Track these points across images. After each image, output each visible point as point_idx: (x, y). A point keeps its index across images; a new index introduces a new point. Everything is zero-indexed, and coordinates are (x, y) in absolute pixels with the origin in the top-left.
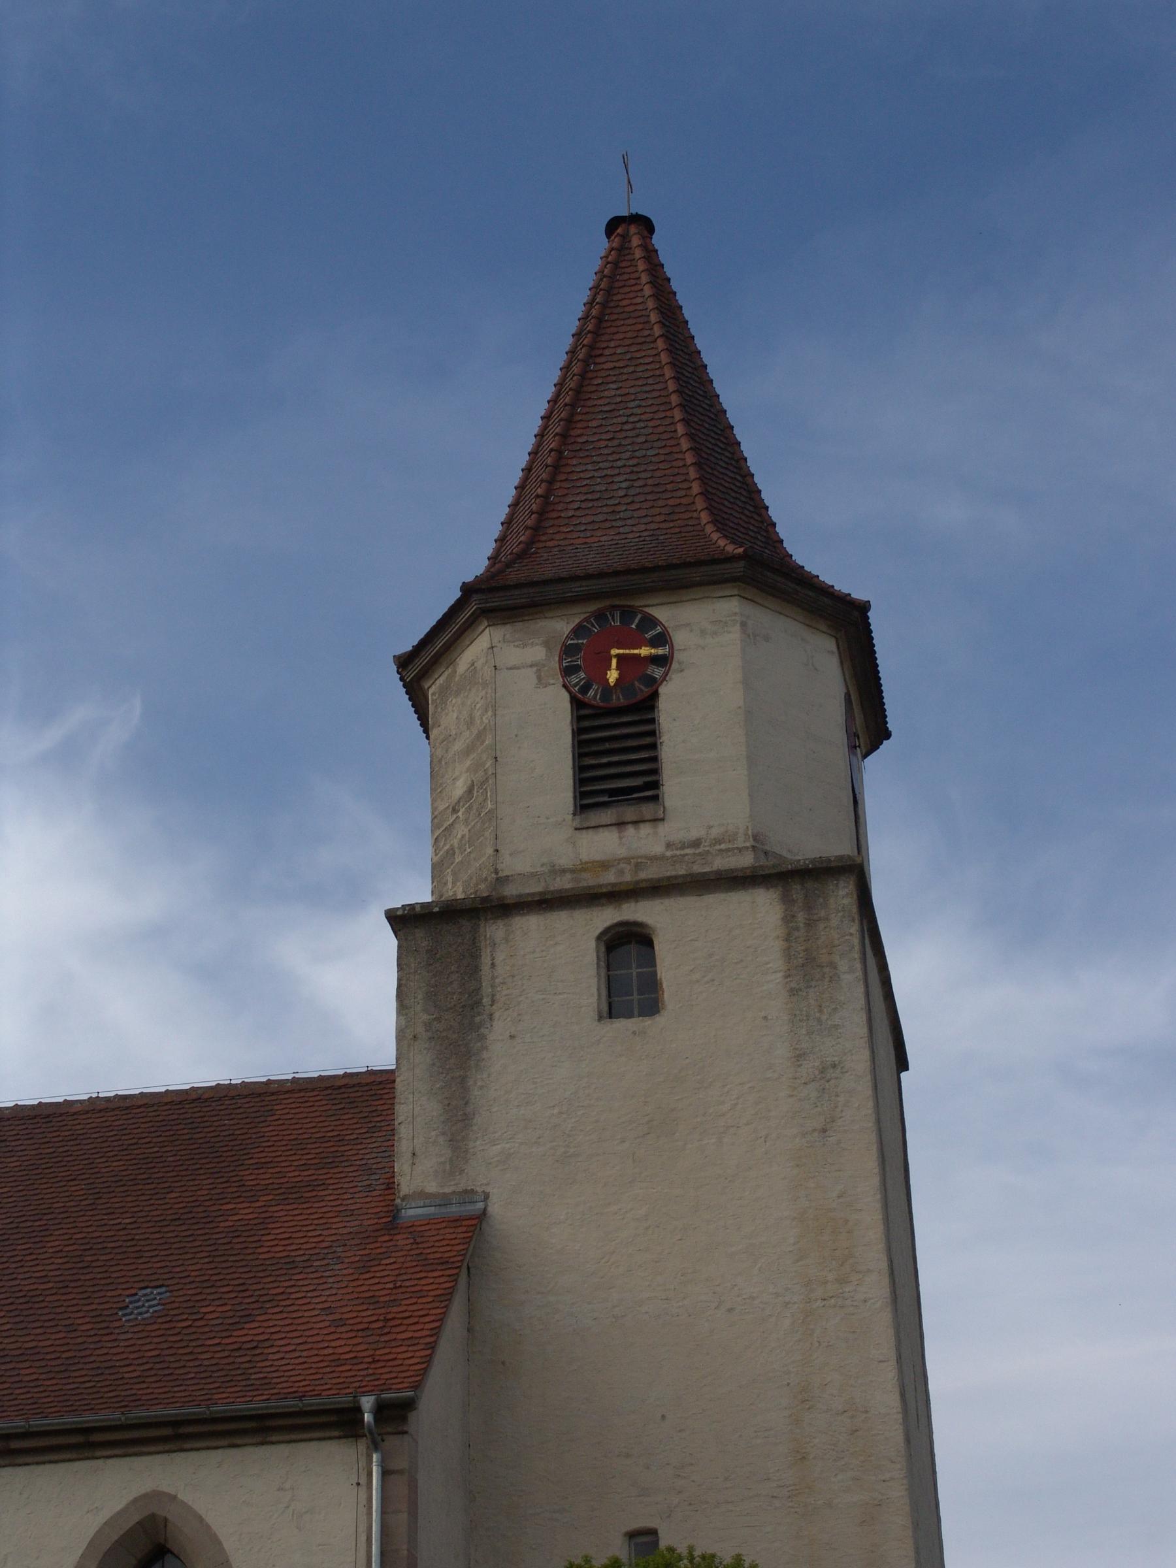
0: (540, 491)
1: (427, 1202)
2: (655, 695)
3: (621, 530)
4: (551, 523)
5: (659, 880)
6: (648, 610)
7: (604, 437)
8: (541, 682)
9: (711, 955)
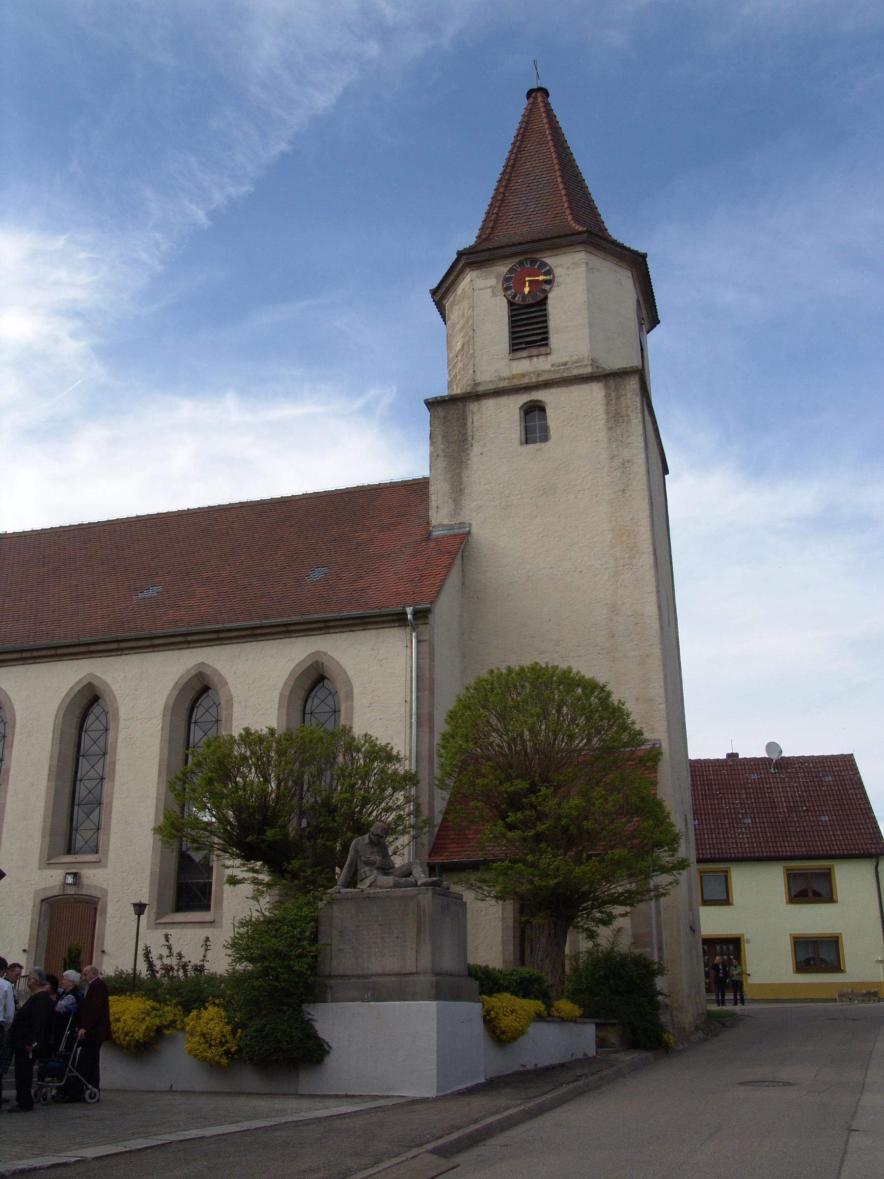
0: (495, 212)
1: (444, 528)
2: (546, 298)
3: (532, 226)
4: (499, 225)
5: (547, 380)
6: (542, 259)
7: (524, 186)
8: (494, 295)
9: (572, 414)
